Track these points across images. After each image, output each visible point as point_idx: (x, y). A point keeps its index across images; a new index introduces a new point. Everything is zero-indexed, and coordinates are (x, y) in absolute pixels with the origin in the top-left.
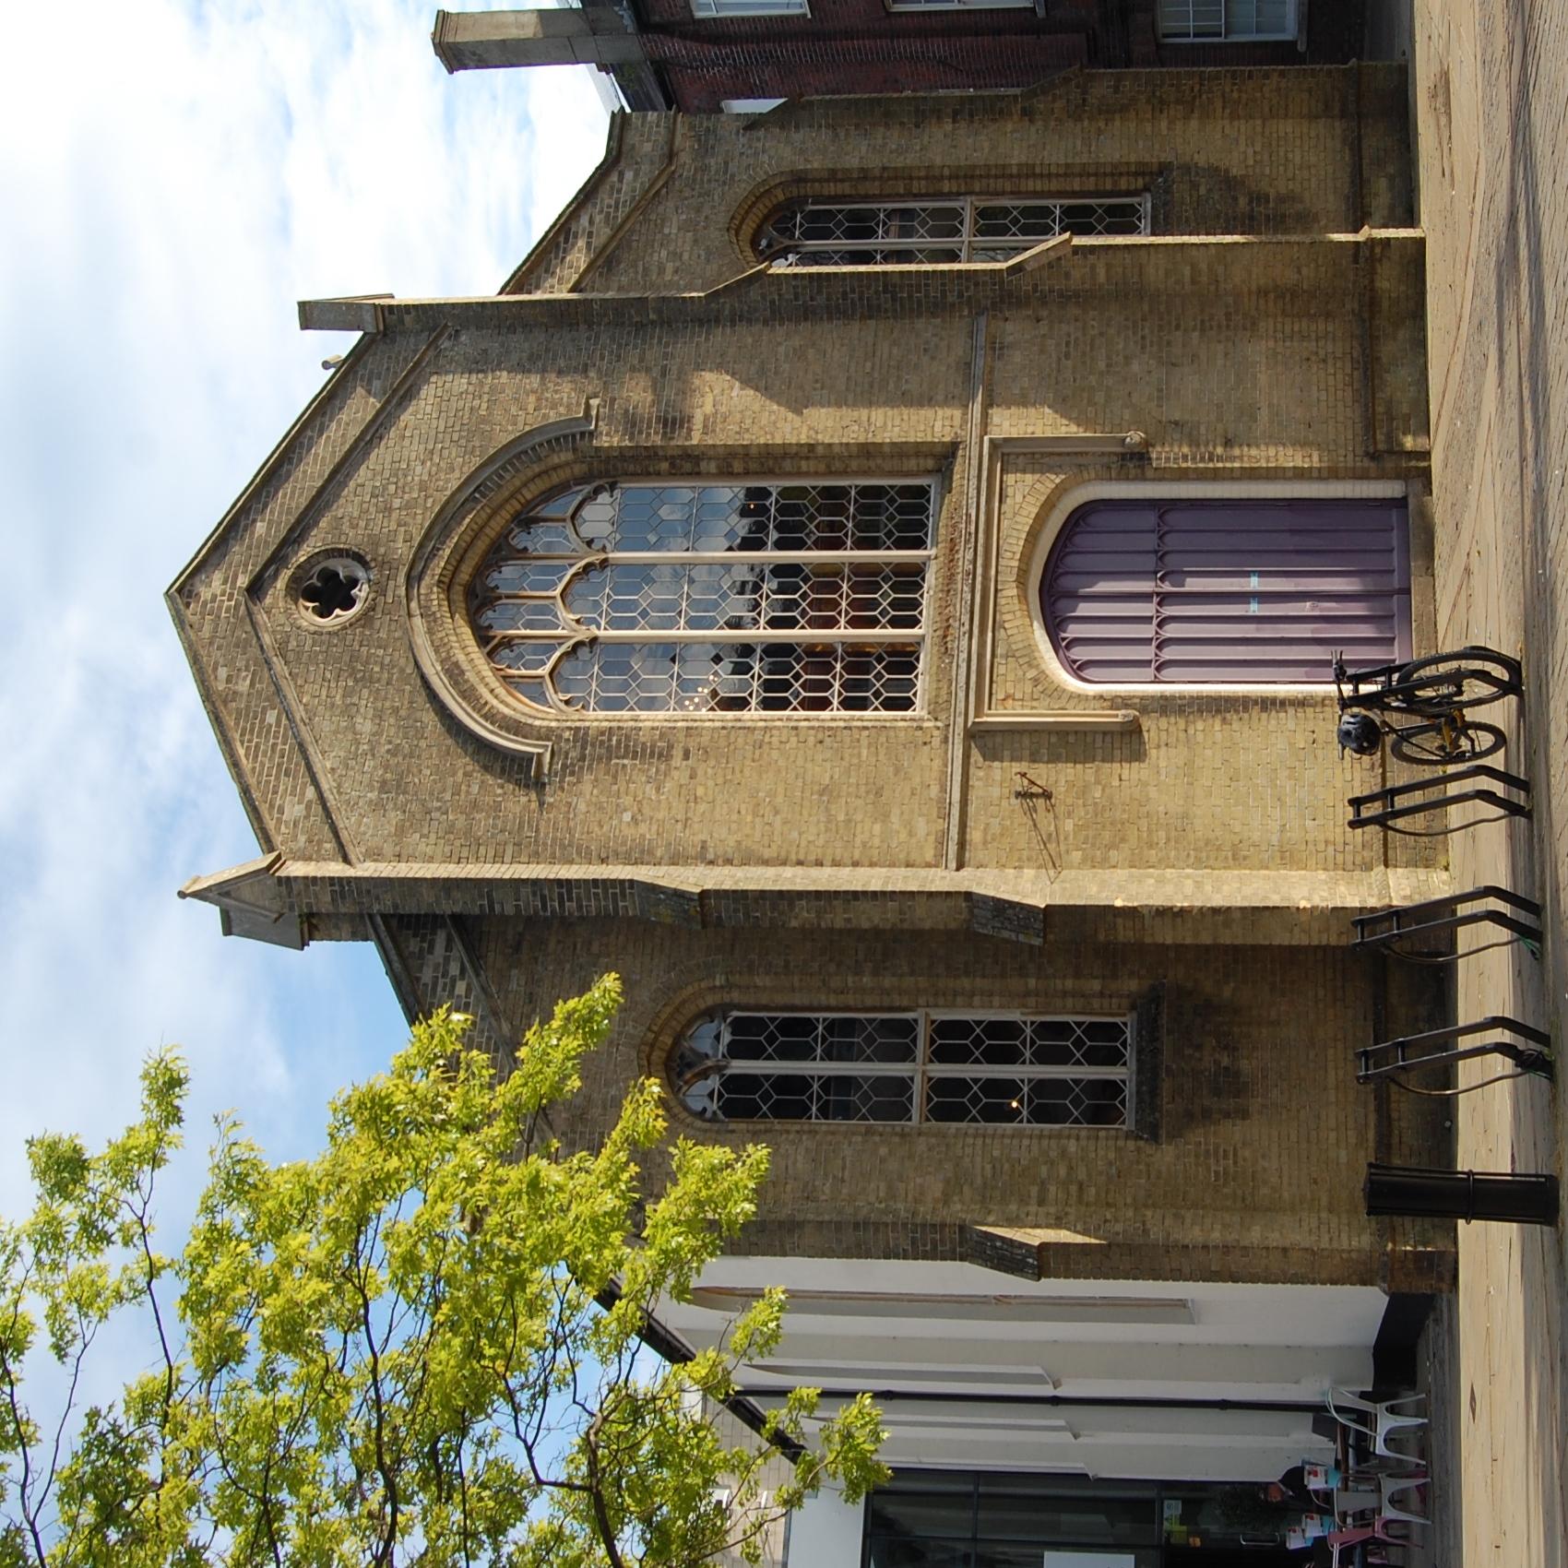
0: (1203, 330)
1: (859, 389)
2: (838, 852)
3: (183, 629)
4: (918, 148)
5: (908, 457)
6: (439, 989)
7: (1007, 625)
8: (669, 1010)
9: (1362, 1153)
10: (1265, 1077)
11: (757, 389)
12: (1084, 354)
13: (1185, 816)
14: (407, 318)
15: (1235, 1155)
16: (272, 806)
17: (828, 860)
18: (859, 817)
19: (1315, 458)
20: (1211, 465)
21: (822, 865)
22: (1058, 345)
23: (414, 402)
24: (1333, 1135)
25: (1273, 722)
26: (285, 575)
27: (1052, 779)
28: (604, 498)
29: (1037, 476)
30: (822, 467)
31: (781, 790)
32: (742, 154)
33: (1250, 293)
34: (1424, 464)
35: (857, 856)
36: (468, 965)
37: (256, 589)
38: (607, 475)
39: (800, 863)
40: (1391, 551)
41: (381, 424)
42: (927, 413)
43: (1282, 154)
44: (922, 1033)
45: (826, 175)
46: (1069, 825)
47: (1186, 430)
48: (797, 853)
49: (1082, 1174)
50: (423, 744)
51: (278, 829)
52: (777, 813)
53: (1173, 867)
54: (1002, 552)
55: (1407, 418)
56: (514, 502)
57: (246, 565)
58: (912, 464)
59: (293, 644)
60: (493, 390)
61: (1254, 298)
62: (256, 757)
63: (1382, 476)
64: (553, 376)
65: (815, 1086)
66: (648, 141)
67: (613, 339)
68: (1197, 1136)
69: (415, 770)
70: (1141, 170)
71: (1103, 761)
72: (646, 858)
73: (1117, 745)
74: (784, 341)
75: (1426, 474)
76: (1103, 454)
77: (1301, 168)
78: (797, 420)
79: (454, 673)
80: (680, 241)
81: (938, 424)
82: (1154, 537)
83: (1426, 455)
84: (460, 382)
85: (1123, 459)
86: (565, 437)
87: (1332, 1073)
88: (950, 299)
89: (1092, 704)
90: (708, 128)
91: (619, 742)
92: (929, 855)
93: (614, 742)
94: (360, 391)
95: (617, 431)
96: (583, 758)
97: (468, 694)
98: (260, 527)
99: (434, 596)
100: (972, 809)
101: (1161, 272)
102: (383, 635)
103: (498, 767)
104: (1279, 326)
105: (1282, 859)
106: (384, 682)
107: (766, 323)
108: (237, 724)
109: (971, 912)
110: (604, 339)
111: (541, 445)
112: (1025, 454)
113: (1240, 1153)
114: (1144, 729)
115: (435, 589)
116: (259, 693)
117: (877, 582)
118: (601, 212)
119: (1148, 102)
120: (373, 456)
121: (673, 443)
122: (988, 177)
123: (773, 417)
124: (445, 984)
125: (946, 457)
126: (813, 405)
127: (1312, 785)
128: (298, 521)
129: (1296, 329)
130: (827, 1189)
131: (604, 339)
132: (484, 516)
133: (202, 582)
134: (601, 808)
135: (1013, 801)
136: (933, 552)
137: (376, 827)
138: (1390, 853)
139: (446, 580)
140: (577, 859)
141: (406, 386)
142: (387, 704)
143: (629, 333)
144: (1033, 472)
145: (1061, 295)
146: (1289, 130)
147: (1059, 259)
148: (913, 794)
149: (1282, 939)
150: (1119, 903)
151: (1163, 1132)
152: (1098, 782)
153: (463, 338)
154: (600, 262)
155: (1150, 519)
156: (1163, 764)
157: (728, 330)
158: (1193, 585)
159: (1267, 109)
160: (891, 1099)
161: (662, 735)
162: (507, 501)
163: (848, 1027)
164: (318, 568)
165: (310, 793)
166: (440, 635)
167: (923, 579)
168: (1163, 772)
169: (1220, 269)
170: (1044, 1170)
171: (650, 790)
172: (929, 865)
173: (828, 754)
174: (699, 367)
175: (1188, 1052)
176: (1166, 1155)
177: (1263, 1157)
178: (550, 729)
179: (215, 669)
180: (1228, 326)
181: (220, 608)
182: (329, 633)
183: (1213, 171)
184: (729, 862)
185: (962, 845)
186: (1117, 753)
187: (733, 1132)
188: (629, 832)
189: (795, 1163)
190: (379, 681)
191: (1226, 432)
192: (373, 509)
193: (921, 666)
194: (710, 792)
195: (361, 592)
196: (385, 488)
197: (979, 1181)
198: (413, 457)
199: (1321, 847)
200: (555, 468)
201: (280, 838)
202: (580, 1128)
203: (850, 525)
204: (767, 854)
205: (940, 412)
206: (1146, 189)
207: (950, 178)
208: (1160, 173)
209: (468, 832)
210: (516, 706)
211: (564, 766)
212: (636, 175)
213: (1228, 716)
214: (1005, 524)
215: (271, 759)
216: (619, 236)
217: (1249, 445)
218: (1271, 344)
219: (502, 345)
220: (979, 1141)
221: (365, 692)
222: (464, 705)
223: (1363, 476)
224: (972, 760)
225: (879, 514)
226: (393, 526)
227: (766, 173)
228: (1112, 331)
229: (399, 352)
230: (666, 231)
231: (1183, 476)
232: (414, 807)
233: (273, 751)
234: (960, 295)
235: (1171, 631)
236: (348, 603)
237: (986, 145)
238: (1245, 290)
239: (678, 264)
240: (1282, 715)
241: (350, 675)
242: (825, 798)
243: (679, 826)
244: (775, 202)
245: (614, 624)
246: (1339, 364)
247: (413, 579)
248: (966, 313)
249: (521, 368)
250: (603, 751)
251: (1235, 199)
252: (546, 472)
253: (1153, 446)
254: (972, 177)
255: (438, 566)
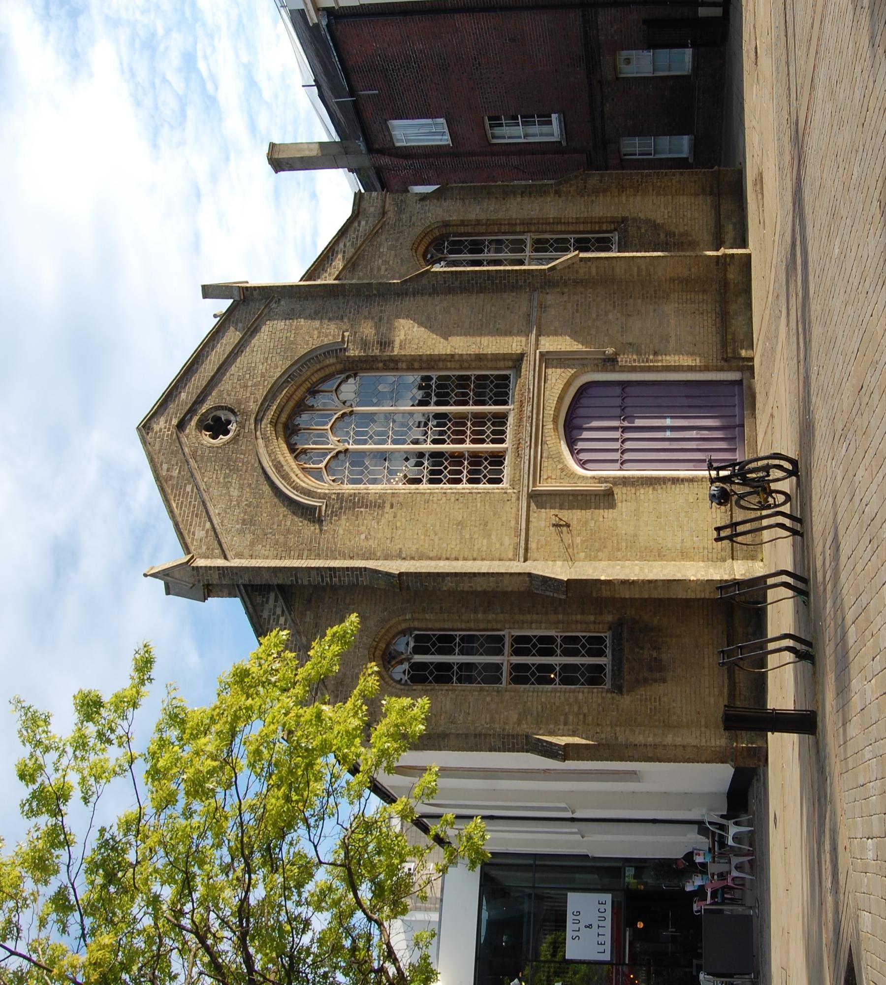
0: (643, 299)
1: (475, 328)
2: (466, 553)
3: (146, 445)
4: (504, 209)
5: (500, 360)
6: (271, 621)
7: (548, 443)
8: (383, 631)
9: (721, 699)
10: (674, 662)
11: (426, 327)
12: (585, 309)
13: (635, 535)
14: (255, 293)
15: (660, 700)
16: (189, 531)
17: (461, 557)
18: (476, 536)
19: (698, 361)
20: (647, 364)
21: (458, 560)
22: (573, 306)
23: (258, 334)
24: (707, 690)
25: (678, 489)
26: (195, 419)
27: (570, 518)
28: (351, 380)
29: (563, 370)
30: (458, 366)
31: (438, 524)
32: (418, 213)
33: (666, 280)
34: (751, 364)
35: (475, 555)
36: (285, 609)
37: (181, 426)
38: (353, 369)
39: (447, 559)
40: (735, 406)
41: (242, 345)
42: (508, 339)
43: (681, 213)
44: (507, 641)
45: (459, 223)
46: (578, 540)
47: (635, 347)
48: (446, 554)
49: (585, 710)
50: (263, 501)
51: (192, 543)
52: (436, 534)
53: (629, 560)
54: (545, 407)
55: (742, 341)
56: (307, 383)
57: (176, 414)
58: (501, 364)
59: (199, 452)
60: (297, 328)
61: (668, 282)
62: (181, 508)
63: (730, 369)
64: (326, 321)
65: (455, 668)
66: (372, 206)
67: (355, 303)
68: (641, 691)
69: (259, 514)
70: (613, 220)
71: (595, 508)
72: (372, 556)
73: (602, 501)
74: (439, 304)
75: (752, 369)
76: (595, 359)
77: (690, 220)
78: (445, 343)
79: (278, 467)
80: (388, 255)
81: (514, 345)
82: (620, 399)
83: (751, 359)
84: (281, 324)
85: (604, 361)
86: (332, 351)
87: (707, 660)
88: (520, 283)
89: (590, 481)
90: (402, 200)
91: (359, 500)
92: (510, 555)
93: (356, 500)
94: (232, 328)
95: (357, 348)
96: (341, 508)
97: (285, 477)
98: (183, 396)
99: (268, 429)
100: (531, 532)
101: (623, 271)
102: (243, 448)
103: (300, 512)
104: (680, 297)
105: (682, 556)
106: (244, 471)
107: (430, 295)
108: (172, 492)
109: (531, 582)
110: (351, 303)
111: (320, 355)
112: (557, 359)
113: (662, 700)
114: (615, 493)
115: (269, 426)
116: (183, 476)
117: (481, 461)
118: (349, 241)
119: (616, 187)
120: (238, 360)
121: (385, 354)
122: (538, 223)
123: (434, 341)
124: (274, 619)
125: (518, 360)
126: (453, 335)
127: (697, 520)
128: (202, 392)
129: (689, 297)
130: (461, 718)
131: (351, 303)
132: (293, 390)
133: (155, 422)
134: (350, 532)
135: (551, 528)
136: (512, 407)
137: (240, 542)
138: (735, 553)
139: (274, 421)
140: (339, 557)
141: (255, 326)
142: (246, 482)
143: (363, 301)
144: (561, 368)
145: (574, 281)
146: (685, 201)
147: (573, 264)
148: (502, 525)
149: (682, 595)
150: (603, 578)
151: (625, 690)
152: (592, 519)
153: (282, 303)
154: (349, 266)
155: (618, 390)
156: (624, 510)
157: (412, 299)
158: (639, 423)
159: (674, 191)
160: (492, 674)
161: (380, 497)
162: (304, 382)
163: (471, 639)
164: (212, 415)
165: (208, 525)
166: (271, 448)
167: (507, 420)
168: (624, 514)
169: (652, 269)
170: (567, 708)
171: (374, 524)
172: (510, 560)
173: (461, 506)
174: (398, 317)
175: (636, 650)
176: (626, 701)
177: (674, 701)
178: (325, 494)
179: (161, 465)
180: (655, 297)
181: (164, 435)
182: (217, 447)
183: (648, 221)
184: (413, 558)
185: (526, 550)
186: (602, 504)
187: (415, 690)
188: (364, 544)
189: (445, 705)
190: (241, 470)
191: (654, 347)
192: (238, 387)
193: (506, 463)
194: (403, 524)
195: (233, 427)
196: (244, 376)
197: (535, 713)
198: (258, 361)
199: (701, 550)
200: (327, 366)
201: (193, 547)
202: (340, 689)
203: (471, 394)
204: (431, 554)
205: (515, 339)
206: (615, 230)
207: (520, 224)
208: (623, 222)
209: (285, 544)
210: (309, 483)
211: (332, 512)
212: (367, 223)
213: (656, 486)
214: (547, 393)
215: (189, 509)
216: (358, 253)
217: (666, 355)
218: (676, 305)
219: (301, 306)
220: (535, 694)
221: (235, 476)
222: (283, 482)
223: (721, 369)
224: (531, 508)
225: (485, 388)
226: (248, 395)
227: (430, 222)
228: (599, 299)
229: (251, 310)
230: (381, 250)
231: (633, 369)
232: (259, 532)
233: (190, 505)
234: (525, 282)
235: (628, 445)
236: (226, 432)
237: (537, 208)
238: (663, 279)
239: (387, 266)
240: (682, 486)
241: (227, 468)
242: (460, 527)
243: (388, 541)
244: (434, 236)
245: (356, 442)
246: (709, 315)
247: (258, 421)
248: (528, 290)
249: (311, 317)
250: (351, 504)
251: (659, 235)
252: (323, 368)
253: (619, 355)
254: (531, 224)
255: (270, 414)
